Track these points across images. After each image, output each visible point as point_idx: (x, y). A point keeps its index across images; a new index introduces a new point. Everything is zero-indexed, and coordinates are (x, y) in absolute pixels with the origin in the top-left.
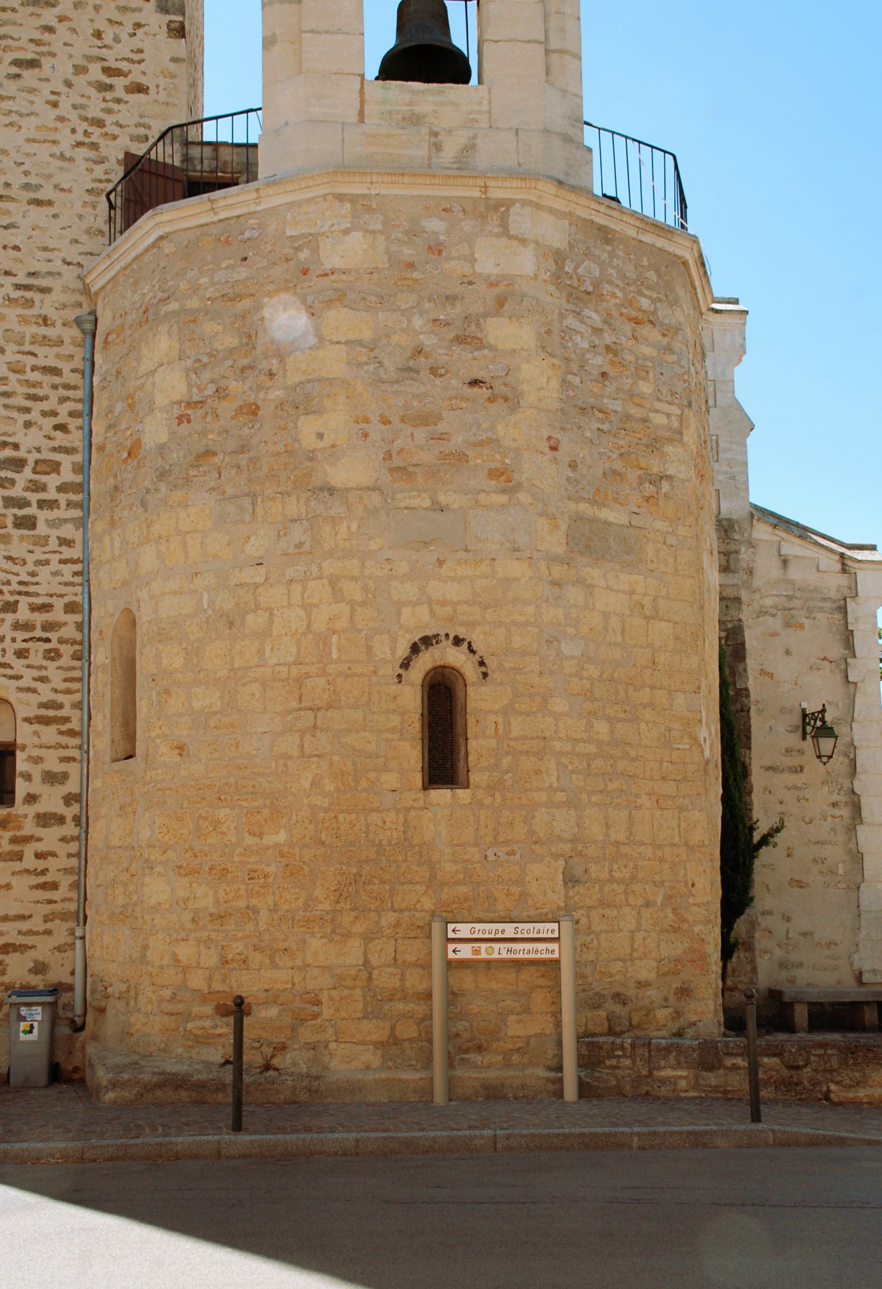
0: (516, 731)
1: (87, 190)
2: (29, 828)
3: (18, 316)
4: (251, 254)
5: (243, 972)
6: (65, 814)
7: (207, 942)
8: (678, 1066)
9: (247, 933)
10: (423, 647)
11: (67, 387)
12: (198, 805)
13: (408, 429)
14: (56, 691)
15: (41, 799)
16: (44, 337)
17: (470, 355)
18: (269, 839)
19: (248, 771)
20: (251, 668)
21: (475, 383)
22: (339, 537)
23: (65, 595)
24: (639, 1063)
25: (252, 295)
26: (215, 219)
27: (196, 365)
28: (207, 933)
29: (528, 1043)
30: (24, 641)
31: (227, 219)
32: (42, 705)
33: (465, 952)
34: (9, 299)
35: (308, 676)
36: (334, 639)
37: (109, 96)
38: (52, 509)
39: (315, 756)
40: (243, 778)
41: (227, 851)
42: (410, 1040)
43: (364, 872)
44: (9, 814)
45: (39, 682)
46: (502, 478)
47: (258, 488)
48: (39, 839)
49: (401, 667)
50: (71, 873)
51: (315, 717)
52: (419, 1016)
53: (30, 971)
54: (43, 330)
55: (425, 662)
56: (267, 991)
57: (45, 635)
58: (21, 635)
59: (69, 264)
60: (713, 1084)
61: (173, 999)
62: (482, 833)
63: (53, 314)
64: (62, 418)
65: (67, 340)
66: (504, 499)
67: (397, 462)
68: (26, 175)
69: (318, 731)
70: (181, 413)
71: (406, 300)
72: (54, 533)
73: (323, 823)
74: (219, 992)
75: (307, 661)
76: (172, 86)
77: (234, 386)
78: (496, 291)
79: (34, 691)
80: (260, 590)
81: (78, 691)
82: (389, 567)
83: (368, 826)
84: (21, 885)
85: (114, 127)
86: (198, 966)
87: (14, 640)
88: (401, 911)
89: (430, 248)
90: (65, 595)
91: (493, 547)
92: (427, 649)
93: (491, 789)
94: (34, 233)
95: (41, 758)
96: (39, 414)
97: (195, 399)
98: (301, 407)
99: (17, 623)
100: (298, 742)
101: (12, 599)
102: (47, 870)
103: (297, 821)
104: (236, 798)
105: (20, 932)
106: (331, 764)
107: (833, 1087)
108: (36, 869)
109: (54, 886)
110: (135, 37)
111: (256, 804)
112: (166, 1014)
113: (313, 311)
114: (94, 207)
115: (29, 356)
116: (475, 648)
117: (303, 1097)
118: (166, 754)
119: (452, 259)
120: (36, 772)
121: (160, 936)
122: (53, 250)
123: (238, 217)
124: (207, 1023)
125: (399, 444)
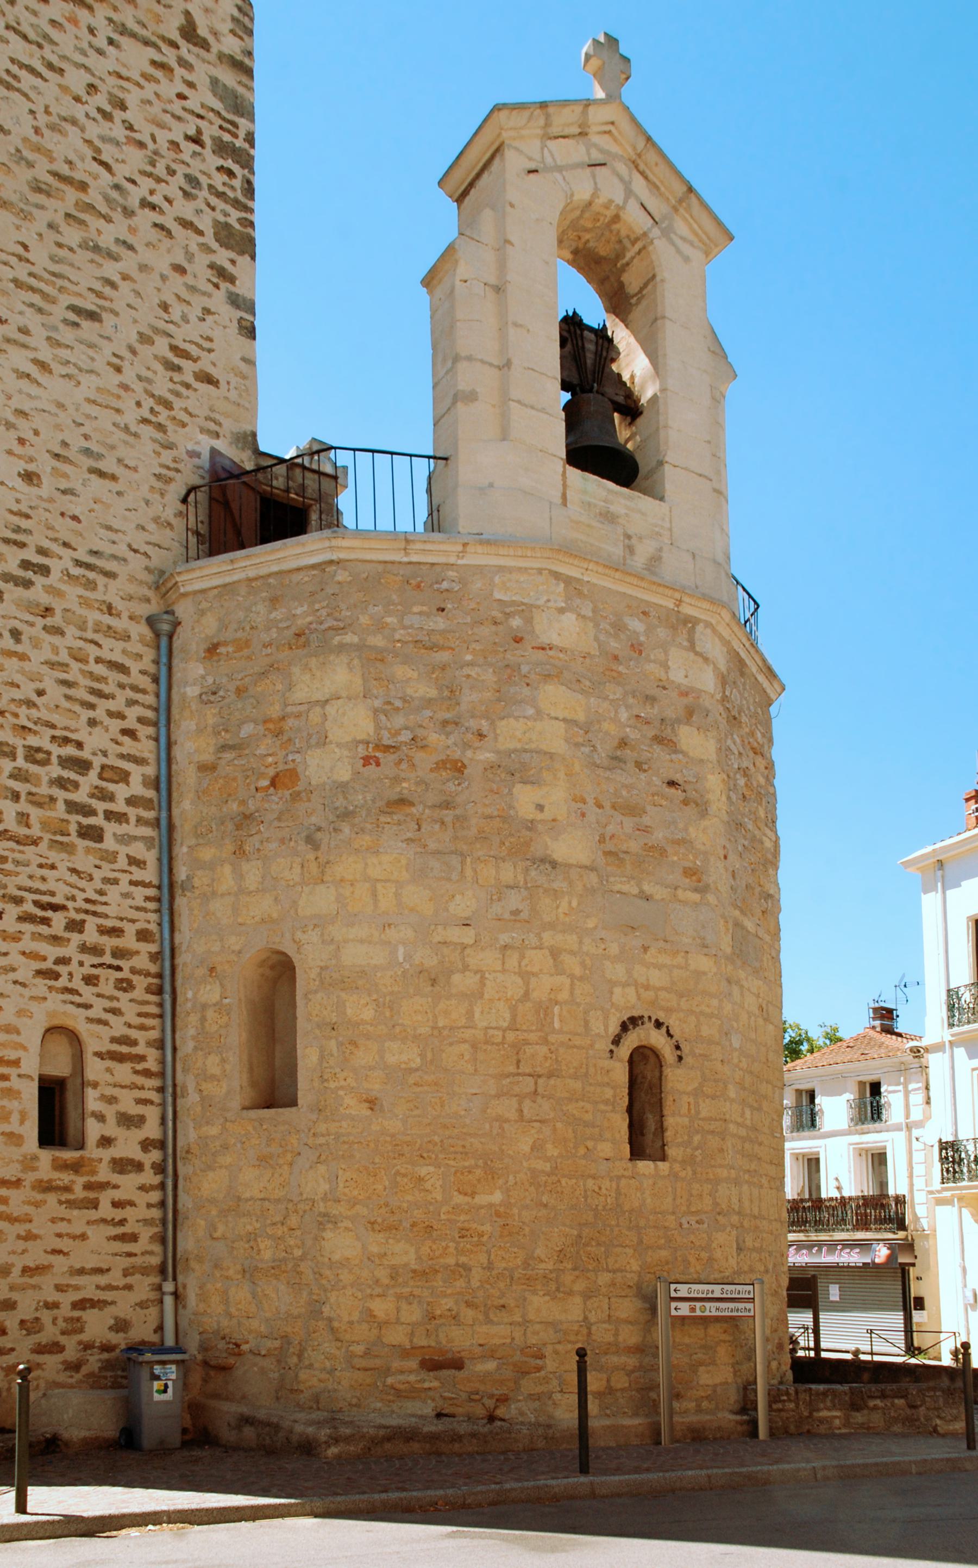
0: (704, 1114)
1: (155, 475)
2: (104, 1174)
3: (80, 597)
4: (449, 606)
5: (454, 1327)
6: (143, 1160)
7: (410, 1298)
8: (834, 1407)
9: (458, 1290)
10: (631, 1027)
11: (135, 689)
12: (395, 1161)
13: (618, 817)
14: (130, 1026)
15: (117, 1143)
16: (109, 627)
17: (668, 756)
18: (481, 1199)
19: (456, 1131)
20: (459, 1028)
21: (672, 783)
22: (560, 910)
23: (138, 921)
24: (802, 1407)
25: (453, 649)
26: (406, 559)
27: (386, 707)
28: (409, 1290)
29: (715, 1391)
30: (93, 966)
31: (419, 563)
32: (114, 1040)
33: (684, 1309)
34: (68, 575)
35: (526, 1042)
36: (556, 1009)
37: (177, 377)
38: (120, 823)
39: (536, 1121)
40: (450, 1137)
41: (431, 1208)
42: (622, 1390)
43: (584, 1235)
44: (82, 1158)
45: (110, 1014)
46: (694, 878)
47: (465, 847)
48: (116, 1187)
49: (613, 1043)
50: (151, 1225)
51: (536, 1083)
52: (629, 1368)
53: (110, 1328)
54: (107, 620)
55: (632, 1040)
56: (481, 1345)
57: (116, 962)
58: (89, 959)
59: (135, 551)
60: (860, 1422)
61: (367, 1354)
62: (678, 1201)
63: (119, 604)
64: (131, 723)
65: (135, 636)
66: (696, 897)
67: (609, 846)
68: (86, 439)
69: (539, 1097)
70: (366, 753)
71: (614, 692)
72: (123, 850)
73: (545, 1186)
74: (423, 1347)
75: (524, 1027)
76: (243, 387)
77: (434, 738)
78: (685, 701)
79: (106, 1023)
80: (468, 951)
81: (153, 1028)
82: (603, 947)
83: (585, 1191)
84: (98, 1235)
85: (182, 413)
86: (398, 1321)
87: (81, 964)
88: (614, 1271)
89: (632, 645)
90: (138, 921)
91: (686, 940)
92: (634, 1028)
93: (688, 1161)
94: (96, 507)
95: (115, 1098)
96: (104, 713)
97: (385, 743)
98: (517, 775)
99: (84, 944)
100: (516, 1106)
101: (79, 917)
102: (125, 1220)
103: (516, 1183)
104: (441, 1156)
105: (98, 1287)
106: (555, 1129)
107: (938, 1422)
108: (113, 1219)
109: (134, 1238)
110: (203, 323)
111: (467, 1164)
112: (359, 1369)
113: (528, 681)
114: (162, 494)
115: (93, 646)
116: (671, 1032)
117: (541, 1444)
118: (352, 1106)
119: (650, 661)
120: (110, 1112)
121: (349, 1292)
122: (117, 531)
123: (433, 564)
124: (412, 1378)
125: (611, 829)
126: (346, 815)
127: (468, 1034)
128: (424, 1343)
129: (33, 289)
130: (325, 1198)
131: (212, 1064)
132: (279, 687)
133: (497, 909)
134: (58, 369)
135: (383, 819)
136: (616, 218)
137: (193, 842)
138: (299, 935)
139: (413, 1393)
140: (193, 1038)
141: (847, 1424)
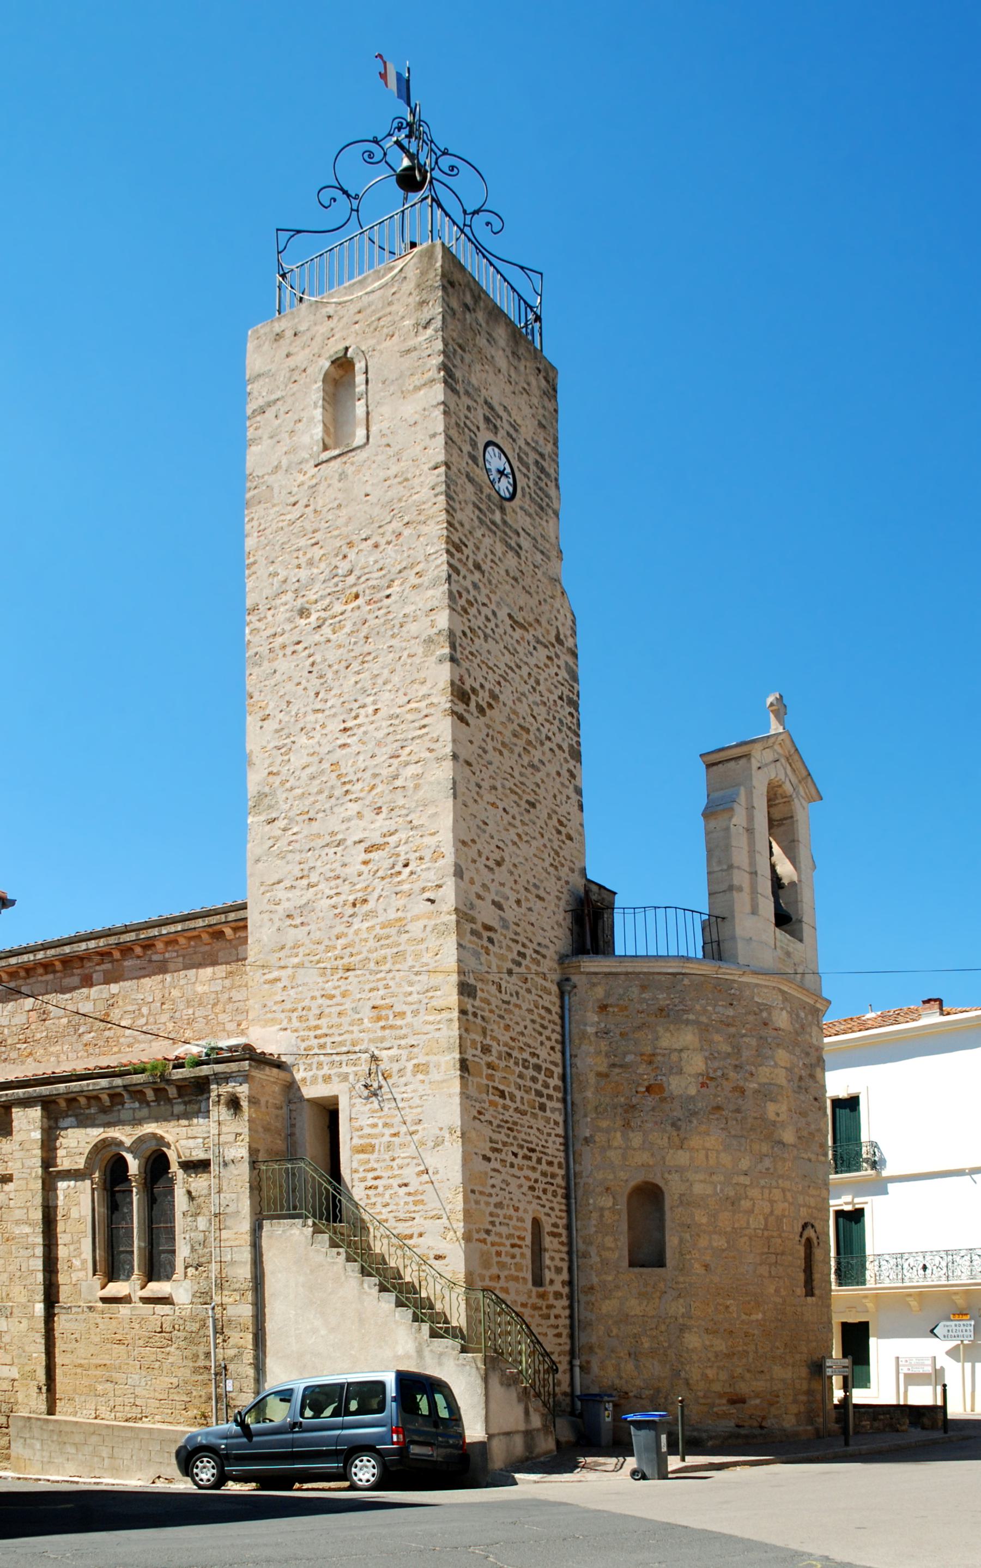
18: (754, 1317)
55: (805, 1236)
61: (705, 1397)
77: (732, 1074)
80: (748, 1188)
93: (821, 1297)
118: (698, 1268)
121: (696, 1365)
124: (724, 1408)
126: (695, 1114)
127: (747, 1232)
128: (729, 1390)
129: (516, 793)
130: (683, 1316)
131: (609, 1241)
132: (650, 1037)
133: (760, 1167)
134: (525, 838)
135: (711, 1117)
136: (780, 786)
137: (594, 1115)
138: (666, 1175)
139: (725, 1415)
140: (595, 1226)
141: (871, 1428)
